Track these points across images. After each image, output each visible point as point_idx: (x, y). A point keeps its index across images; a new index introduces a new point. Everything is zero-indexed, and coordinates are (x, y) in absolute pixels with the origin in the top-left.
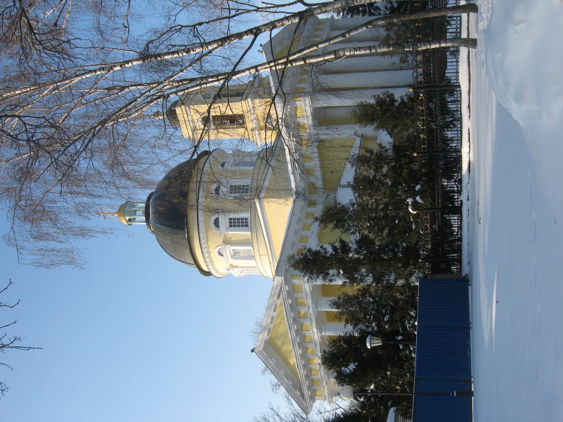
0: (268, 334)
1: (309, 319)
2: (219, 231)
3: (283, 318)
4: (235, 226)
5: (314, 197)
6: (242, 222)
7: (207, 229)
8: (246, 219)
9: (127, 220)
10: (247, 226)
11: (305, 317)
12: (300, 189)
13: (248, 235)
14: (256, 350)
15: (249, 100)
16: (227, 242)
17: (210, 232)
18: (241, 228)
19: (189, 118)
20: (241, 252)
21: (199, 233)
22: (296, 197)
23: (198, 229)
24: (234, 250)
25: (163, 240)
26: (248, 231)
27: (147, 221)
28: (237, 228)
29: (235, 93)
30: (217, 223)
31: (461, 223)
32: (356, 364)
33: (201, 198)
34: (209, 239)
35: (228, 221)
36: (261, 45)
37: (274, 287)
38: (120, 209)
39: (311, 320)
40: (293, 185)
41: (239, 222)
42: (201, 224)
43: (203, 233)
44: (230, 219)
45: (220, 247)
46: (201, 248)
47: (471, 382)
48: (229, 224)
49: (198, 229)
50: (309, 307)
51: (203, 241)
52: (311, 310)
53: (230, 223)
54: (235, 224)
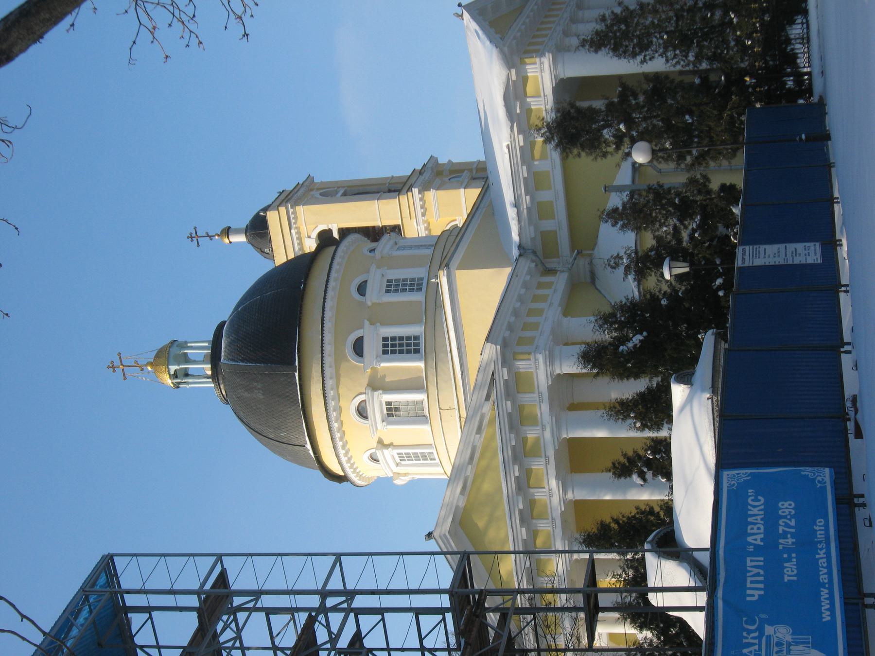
0: (462, 492)
1: (543, 459)
2: (363, 362)
3: (495, 453)
4: (393, 352)
5: (552, 264)
6: (408, 345)
7: (339, 359)
8: (416, 338)
9: (172, 372)
10: (417, 351)
11: (536, 451)
12: (528, 244)
13: (418, 369)
14: (436, 534)
15: (415, 191)
16: (376, 385)
17: (344, 366)
18: (405, 355)
19: (293, 231)
20: (402, 407)
21: (322, 364)
22: (520, 255)
23: (322, 357)
24: (388, 403)
25: (246, 395)
26: (420, 360)
27: (215, 376)
28: (397, 355)
29: (387, 190)
30: (358, 348)
31: (808, 27)
32: (645, 334)
33: (326, 314)
34: (341, 386)
35: (381, 343)
36: (460, 5)
37: (484, 365)
38: (157, 356)
39: (547, 458)
40: (515, 237)
41: (401, 345)
42: (328, 348)
43: (331, 378)
44: (385, 339)
45: (362, 397)
46: (325, 397)
47: (831, 201)
48: (381, 349)
49: (322, 357)
50: (543, 428)
51: (329, 383)
52: (548, 434)
53: (384, 346)
54: (395, 347)
